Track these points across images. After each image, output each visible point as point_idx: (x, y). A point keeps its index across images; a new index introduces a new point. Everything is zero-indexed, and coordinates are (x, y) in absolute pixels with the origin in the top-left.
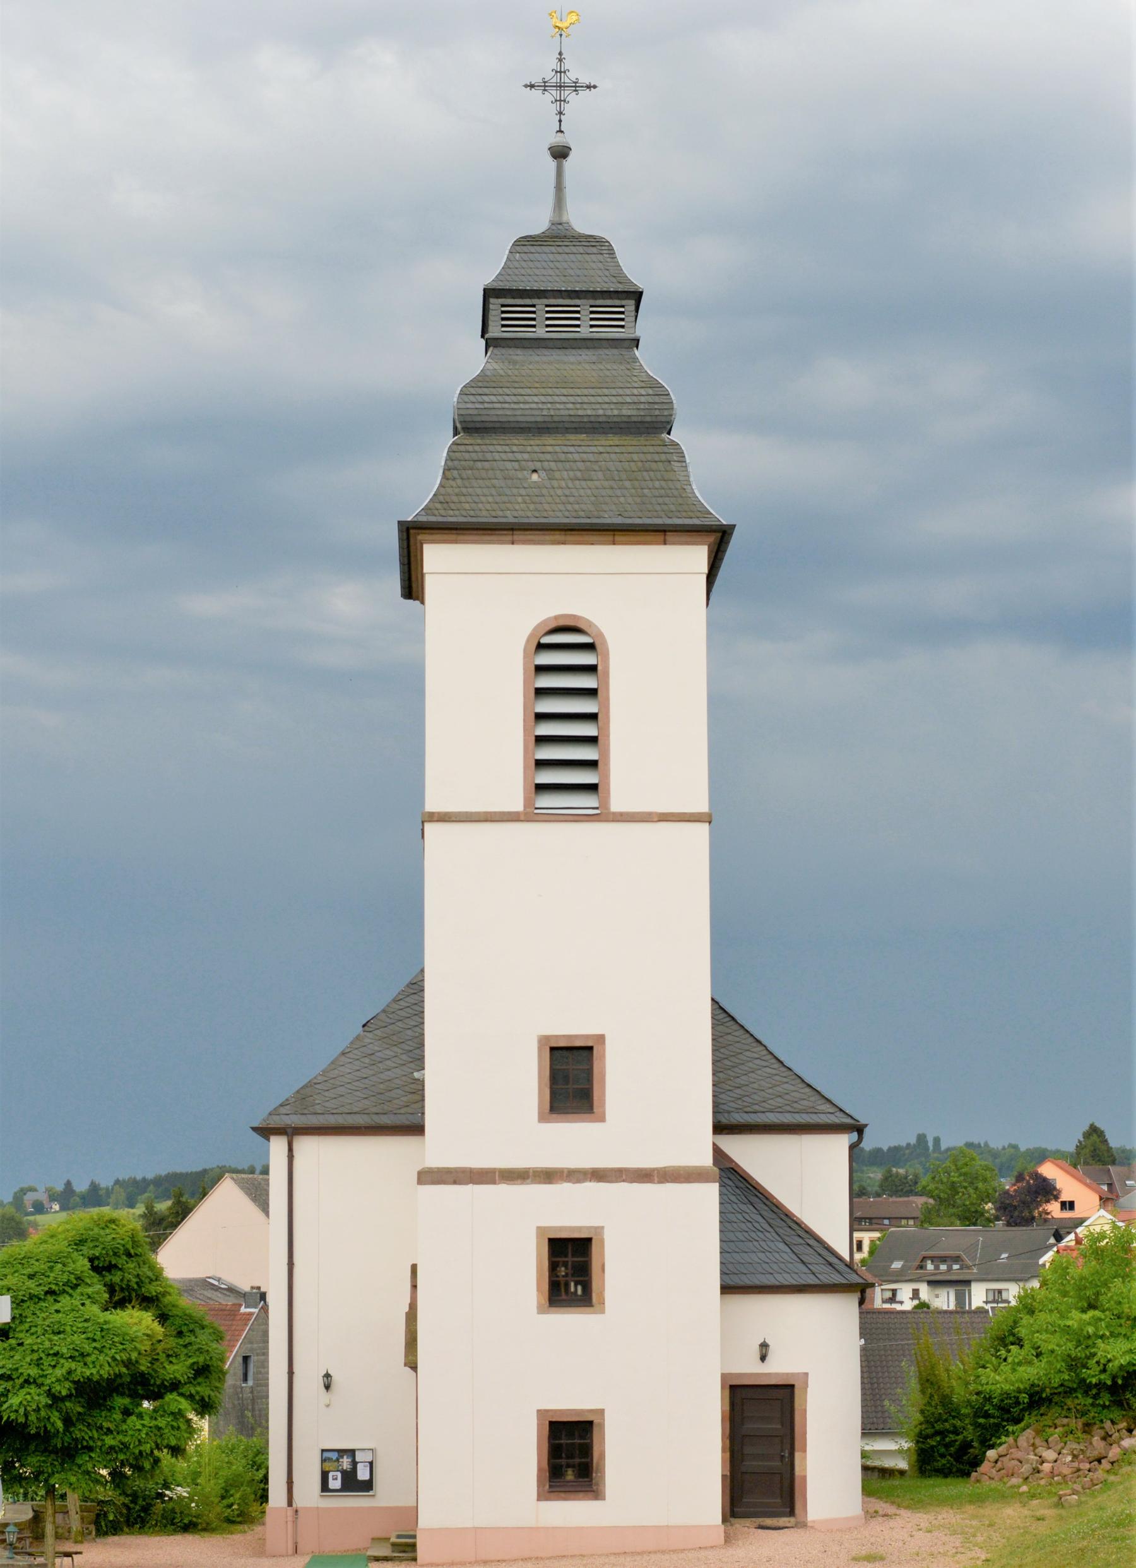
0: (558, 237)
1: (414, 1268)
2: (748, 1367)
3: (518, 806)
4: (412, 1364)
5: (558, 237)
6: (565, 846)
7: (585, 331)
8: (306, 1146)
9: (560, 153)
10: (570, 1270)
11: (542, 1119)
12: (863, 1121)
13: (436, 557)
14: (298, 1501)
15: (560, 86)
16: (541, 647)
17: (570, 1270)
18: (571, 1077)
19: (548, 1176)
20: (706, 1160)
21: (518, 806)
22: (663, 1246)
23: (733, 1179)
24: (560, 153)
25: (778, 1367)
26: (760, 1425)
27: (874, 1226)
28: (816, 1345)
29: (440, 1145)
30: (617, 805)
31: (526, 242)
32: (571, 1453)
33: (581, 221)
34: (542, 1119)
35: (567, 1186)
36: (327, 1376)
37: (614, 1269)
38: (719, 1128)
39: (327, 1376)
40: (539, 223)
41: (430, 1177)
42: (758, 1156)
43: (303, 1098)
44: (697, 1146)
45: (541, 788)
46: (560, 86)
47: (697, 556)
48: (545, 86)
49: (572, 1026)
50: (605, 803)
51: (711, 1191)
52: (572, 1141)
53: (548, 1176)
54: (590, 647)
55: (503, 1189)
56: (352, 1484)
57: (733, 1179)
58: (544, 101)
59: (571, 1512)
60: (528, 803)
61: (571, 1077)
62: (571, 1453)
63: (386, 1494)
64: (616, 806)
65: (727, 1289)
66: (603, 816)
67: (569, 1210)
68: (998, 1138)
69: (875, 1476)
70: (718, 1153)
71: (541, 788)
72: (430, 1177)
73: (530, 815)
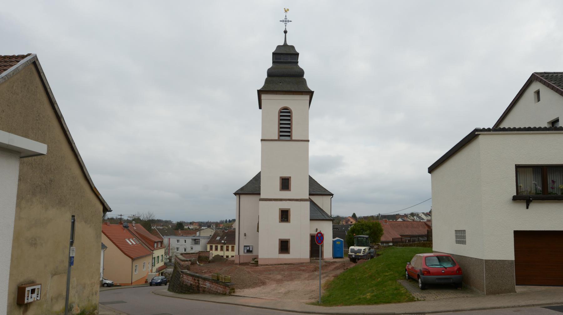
0: (285, 45)
3: (277, 138)
4: (258, 231)
5: (285, 45)
6: (285, 145)
7: (289, 60)
8: (242, 196)
9: (285, 32)
10: (285, 216)
12: (312, 90)
15: (286, 21)
16: (281, 112)
17: (285, 216)
18: (285, 184)
19: (281, 200)
21: (277, 138)
22: (300, 213)
23: (313, 203)
24: (285, 32)
26: (316, 241)
28: (327, 229)
29: (263, 196)
30: (293, 138)
31: (279, 47)
32: (284, 246)
33: (289, 43)
36: (285, 57)
37: (293, 216)
38: (310, 195)
39: (285, 57)
40: (282, 44)
42: (316, 199)
43: (242, 189)
44: (307, 197)
45: (281, 136)
46: (286, 21)
47: (308, 97)
49: (285, 175)
50: (291, 138)
51: (308, 203)
52: (285, 194)
53: (281, 200)
54: (289, 112)
56: (249, 251)
57: (313, 203)
58: (283, 24)
59: (284, 256)
60: (279, 138)
61: (285, 184)
62: (284, 246)
63: (254, 253)
64: (293, 138)
65: (311, 220)
67: (285, 205)
71: (281, 136)
73: (279, 140)
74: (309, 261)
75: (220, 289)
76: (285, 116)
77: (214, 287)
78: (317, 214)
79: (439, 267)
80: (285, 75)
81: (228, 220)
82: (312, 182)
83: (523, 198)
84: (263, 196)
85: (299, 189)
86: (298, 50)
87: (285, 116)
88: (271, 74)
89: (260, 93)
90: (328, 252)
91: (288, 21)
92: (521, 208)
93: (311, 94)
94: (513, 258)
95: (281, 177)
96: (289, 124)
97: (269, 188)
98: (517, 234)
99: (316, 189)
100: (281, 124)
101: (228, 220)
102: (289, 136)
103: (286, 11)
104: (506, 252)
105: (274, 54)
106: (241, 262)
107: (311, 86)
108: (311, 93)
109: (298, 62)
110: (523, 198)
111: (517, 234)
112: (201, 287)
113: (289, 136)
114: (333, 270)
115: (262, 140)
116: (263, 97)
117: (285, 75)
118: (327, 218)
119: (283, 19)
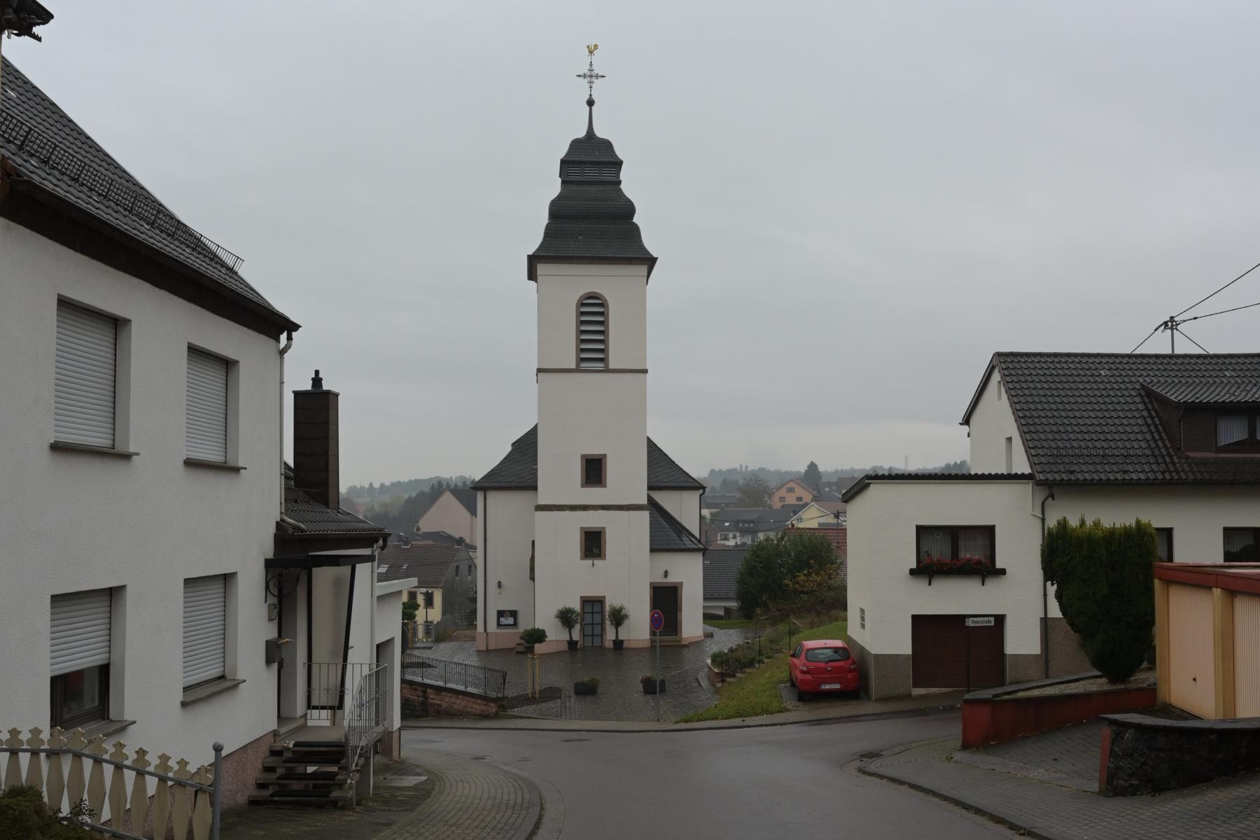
1: (533, 542)
2: (660, 579)
3: (573, 366)
4: (533, 579)
9: (591, 103)
10: (593, 544)
11: (583, 486)
13: (541, 269)
14: (489, 630)
15: (591, 76)
16: (583, 305)
17: (593, 544)
18: (594, 470)
19: (584, 508)
20: (644, 501)
21: (573, 366)
22: (629, 535)
23: (653, 505)
24: (591, 103)
25: (672, 579)
26: (665, 600)
27: (136, 188)
28: (688, 573)
30: (611, 366)
33: (600, 133)
34: (583, 486)
35: (592, 512)
38: (650, 488)
40: (581, 133)
41: (540, 508)
45: (583, 360)
46: (591, 76)
47: (644, 269)
48: (585, 76)
50: (607, 365)
51: (645, 515)
52: (594, 495)
53: (584, 508)
54: (601, 305)
55: (568, 513)
57: (653, 505)
58: (585, 82)
60: (578, 365)
61: (594, 470)
64: (611, 366)
65: (652, 550)
66: (607, 370)
67: (592, 520)
68: (433, 476)
69: (708, 618)
70: (650, 499)
71: (583, 360)
72: (540, 508)
73: (578, 370)
74: (648, 644)
75: (493, 708)
76: (593, 312)
77: (459, 703)
78: (667, 536)
79: (841, 664)
80: (592, 217)
81: (376, 485)
82: (655, 455)
83: (926, 570)
84: (544, 497)
85: (628, 479)
86: (620, 152)
87: (593, 312)
88: (558, 211)
89: (533, 261)
90: (692, 624)
91: (597, 76)
92: (921, 585)
93: (650, 262)
94: (909, 652)
95: (583, 456)
96: (601, 332)
97: (558, 475)
98: (917, 620)
99: (664, 472)
100: (583, 313)
101: (376, 485)
102: (601, 360)
103: (591, 52)
104: (904, 646)
105: (563, 162)
106: (491, 647)
107: (650, 242)
108: (650, 262)
109: (620, 182)
110: (926, 570)
111: (917, 620)
112: (433, 705)
113: (601, 360)
114: (170, 830)
115: (539, 370)
116: (541, 269)
117: (592, 217)
118: (690, 546)
119: (585, 70)
